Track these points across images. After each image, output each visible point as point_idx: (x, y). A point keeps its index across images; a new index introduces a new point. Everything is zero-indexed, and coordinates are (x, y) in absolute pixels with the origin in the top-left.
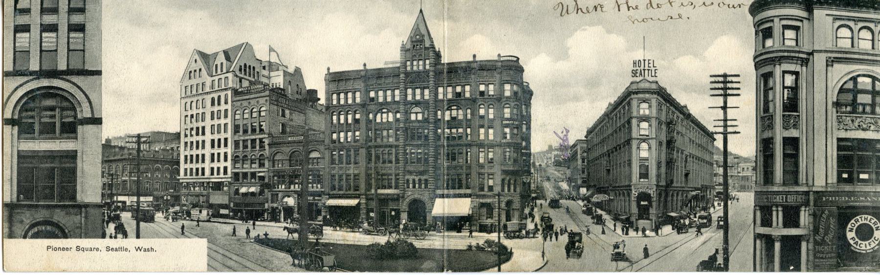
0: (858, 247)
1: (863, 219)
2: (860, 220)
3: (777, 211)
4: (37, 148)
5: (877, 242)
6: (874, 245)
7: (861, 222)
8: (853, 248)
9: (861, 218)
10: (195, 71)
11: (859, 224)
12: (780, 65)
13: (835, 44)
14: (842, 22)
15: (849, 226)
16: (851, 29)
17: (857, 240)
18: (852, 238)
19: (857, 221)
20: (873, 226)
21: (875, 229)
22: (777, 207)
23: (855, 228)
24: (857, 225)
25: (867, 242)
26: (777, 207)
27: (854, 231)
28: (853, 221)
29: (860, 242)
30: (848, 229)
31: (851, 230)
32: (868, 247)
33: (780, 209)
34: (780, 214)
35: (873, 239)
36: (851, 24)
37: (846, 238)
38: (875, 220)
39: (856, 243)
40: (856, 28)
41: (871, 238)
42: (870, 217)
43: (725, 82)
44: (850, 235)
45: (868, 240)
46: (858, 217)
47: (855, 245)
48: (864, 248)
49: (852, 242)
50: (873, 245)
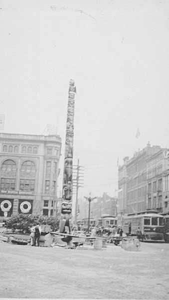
49: (2, 208)
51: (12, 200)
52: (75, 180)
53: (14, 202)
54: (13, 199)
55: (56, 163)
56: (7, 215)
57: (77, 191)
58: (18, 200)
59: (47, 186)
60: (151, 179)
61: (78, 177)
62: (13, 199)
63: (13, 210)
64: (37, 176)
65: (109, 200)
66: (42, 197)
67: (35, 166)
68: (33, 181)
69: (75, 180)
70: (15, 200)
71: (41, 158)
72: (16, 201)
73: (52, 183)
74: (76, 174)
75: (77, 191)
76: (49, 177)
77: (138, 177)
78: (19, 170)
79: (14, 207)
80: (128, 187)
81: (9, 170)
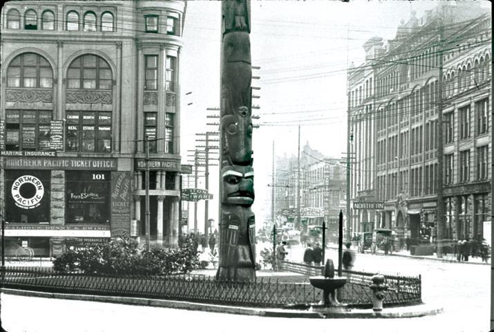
0: (21, 204)
1: (35, 181)
2: (24, 180)
3: (161, 175)
4: (149, 208)
5: (39, 200)
6: (37, 202)
7: (25, 182)
8: (17, 205)
9: (25, 178)
10: (423, 72)
11: (23, 183)
12: (142, 50)
13: (65, 28)
14: (72, 8)
15: (14, 185)
16: (77, 13)
17: (21, 197)
18: (16, 196)
19: (21, 180)
20: (35, 185)
21: (37, 188)
22: (162, 171)
23: (19, 187)
24: (21, 184)
25: (30, 200)
26: (162, 171)
27: (18, 189)
28: (17, 181)
29: (23, 199)
30: (13, 188)
31: (15, 189)
32: (31, 204)
33: (164, 173)
34: (164, 177)
35: (35, 197)
36: (78, 9)
37: (11, 195)
38: (38, 180)
39: (20, 200)
40: (99, 14)
41: (33, 196)
42: (33, 177)
43: (423, 66)
44: (15, 193)
45: (31, 197)
46: (22, 177)
47: (18, 202)
48: (27, 205)
49: (16, 199)
50: (35, 202)
51: (44, 175)
52: (214, 148)
53: (53, 181)
54: (49, 171)
55: (173, 58)
56: (62, 213)
57: (196, 181)
58: (63, 172)
59: (147, 125)
60: (484, 84)
61: (207, 159)
62: (49, 171)
63: (53, 203)
64: (116, 100)
65: (322, 165)
66: (136, 160)
67: (110, 68)
68: (155, 142)
69: (214, 148)
70: (54, 173)
71: (128, 48)
72: (60, 176)
73: (164, 119)
74: (210, 156)
75: (196, 181)
76: (156, 102)
77: (412, 96)
78: (60, 82)
79: (53, 195)
80: (378, 127)
81: (29, 83)
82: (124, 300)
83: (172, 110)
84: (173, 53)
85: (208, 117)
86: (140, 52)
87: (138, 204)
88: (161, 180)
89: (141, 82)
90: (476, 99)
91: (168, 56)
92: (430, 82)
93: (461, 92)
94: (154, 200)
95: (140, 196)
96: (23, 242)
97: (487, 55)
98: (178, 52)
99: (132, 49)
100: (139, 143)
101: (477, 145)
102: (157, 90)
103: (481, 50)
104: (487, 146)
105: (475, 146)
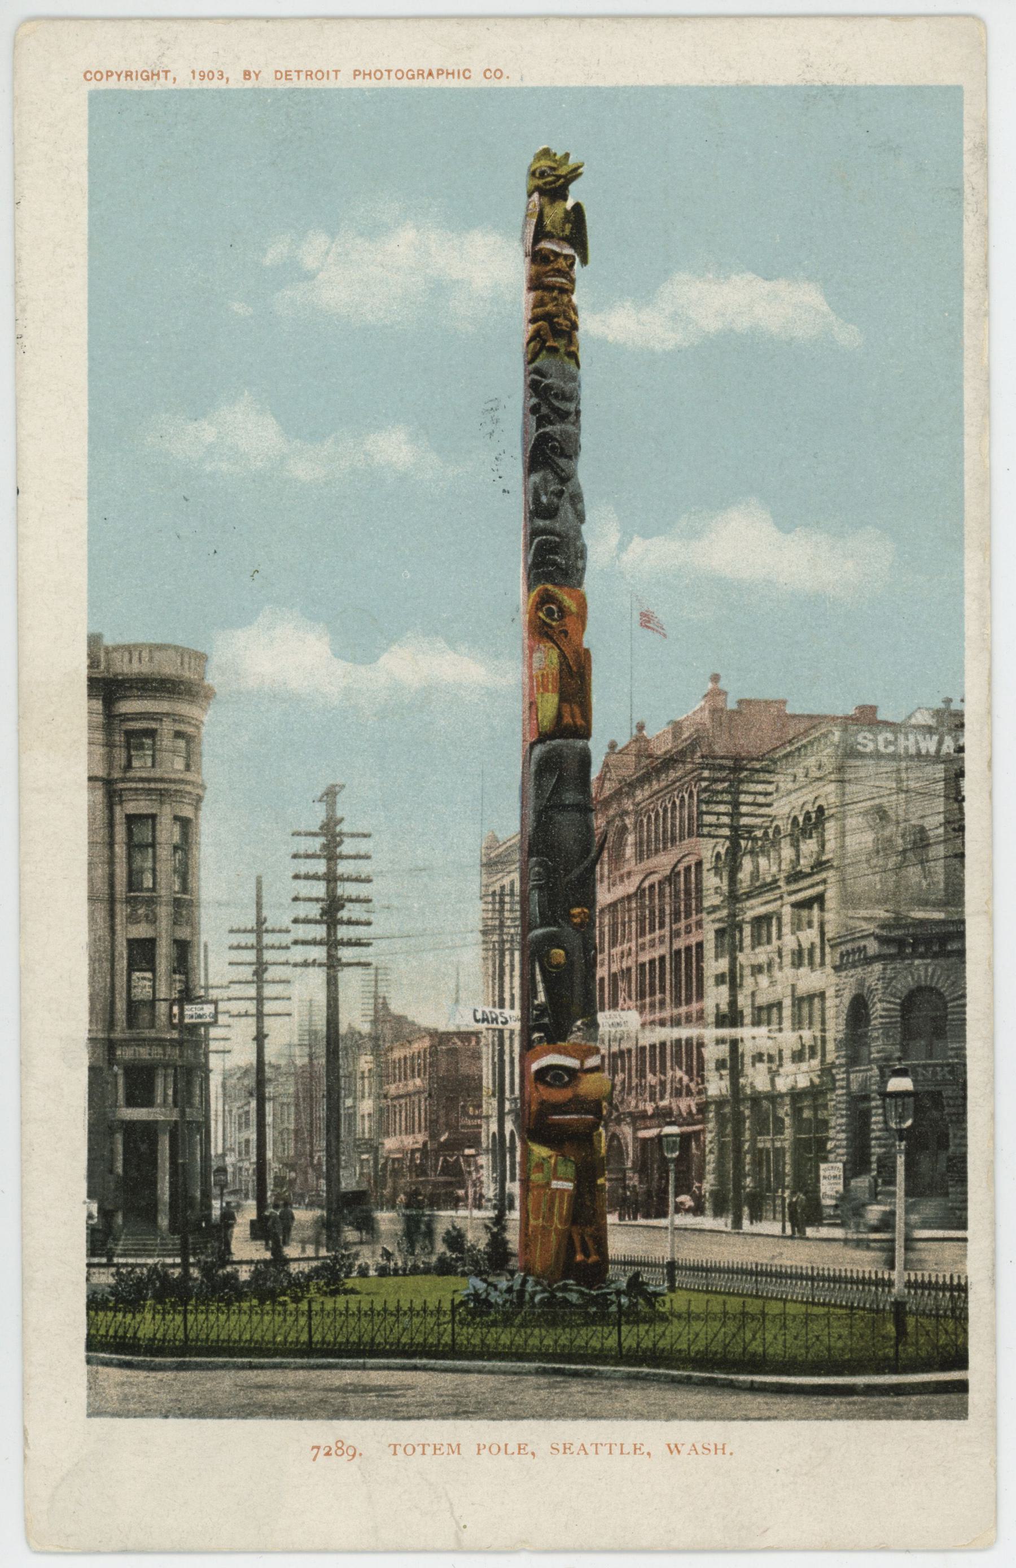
3: (166, 1076)
76: (152, 920)
82: (392, 1365)
83: (184, 933)
84: (187, 812)
85: (230, 964)
86: (118, 809)
87: (119, 1137)
88: (163, 1088)
89: (121, 871)
90: (794, 898)
91: (176, 818)
92: (646, 884)
93: (758, 884)
94: (149, 1130)
95: (123, 1122)
96: (760, 1145)
97: (808, 813)
98: (197, 809)
99: (92, 809)
100: (716, 817)
101: (757, 1004)
102: (154, 889)
103: (805, 799)
104: (779, 1005)
105: (753, 1005)
